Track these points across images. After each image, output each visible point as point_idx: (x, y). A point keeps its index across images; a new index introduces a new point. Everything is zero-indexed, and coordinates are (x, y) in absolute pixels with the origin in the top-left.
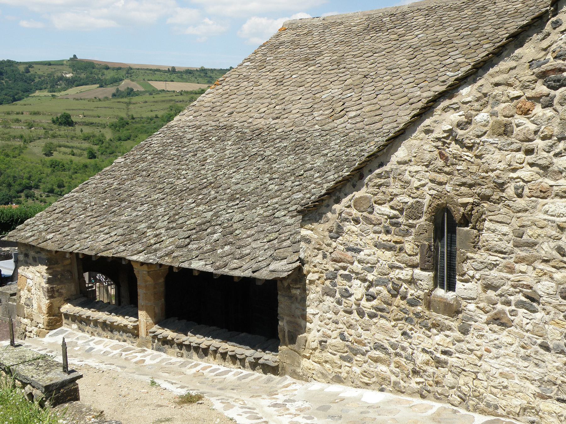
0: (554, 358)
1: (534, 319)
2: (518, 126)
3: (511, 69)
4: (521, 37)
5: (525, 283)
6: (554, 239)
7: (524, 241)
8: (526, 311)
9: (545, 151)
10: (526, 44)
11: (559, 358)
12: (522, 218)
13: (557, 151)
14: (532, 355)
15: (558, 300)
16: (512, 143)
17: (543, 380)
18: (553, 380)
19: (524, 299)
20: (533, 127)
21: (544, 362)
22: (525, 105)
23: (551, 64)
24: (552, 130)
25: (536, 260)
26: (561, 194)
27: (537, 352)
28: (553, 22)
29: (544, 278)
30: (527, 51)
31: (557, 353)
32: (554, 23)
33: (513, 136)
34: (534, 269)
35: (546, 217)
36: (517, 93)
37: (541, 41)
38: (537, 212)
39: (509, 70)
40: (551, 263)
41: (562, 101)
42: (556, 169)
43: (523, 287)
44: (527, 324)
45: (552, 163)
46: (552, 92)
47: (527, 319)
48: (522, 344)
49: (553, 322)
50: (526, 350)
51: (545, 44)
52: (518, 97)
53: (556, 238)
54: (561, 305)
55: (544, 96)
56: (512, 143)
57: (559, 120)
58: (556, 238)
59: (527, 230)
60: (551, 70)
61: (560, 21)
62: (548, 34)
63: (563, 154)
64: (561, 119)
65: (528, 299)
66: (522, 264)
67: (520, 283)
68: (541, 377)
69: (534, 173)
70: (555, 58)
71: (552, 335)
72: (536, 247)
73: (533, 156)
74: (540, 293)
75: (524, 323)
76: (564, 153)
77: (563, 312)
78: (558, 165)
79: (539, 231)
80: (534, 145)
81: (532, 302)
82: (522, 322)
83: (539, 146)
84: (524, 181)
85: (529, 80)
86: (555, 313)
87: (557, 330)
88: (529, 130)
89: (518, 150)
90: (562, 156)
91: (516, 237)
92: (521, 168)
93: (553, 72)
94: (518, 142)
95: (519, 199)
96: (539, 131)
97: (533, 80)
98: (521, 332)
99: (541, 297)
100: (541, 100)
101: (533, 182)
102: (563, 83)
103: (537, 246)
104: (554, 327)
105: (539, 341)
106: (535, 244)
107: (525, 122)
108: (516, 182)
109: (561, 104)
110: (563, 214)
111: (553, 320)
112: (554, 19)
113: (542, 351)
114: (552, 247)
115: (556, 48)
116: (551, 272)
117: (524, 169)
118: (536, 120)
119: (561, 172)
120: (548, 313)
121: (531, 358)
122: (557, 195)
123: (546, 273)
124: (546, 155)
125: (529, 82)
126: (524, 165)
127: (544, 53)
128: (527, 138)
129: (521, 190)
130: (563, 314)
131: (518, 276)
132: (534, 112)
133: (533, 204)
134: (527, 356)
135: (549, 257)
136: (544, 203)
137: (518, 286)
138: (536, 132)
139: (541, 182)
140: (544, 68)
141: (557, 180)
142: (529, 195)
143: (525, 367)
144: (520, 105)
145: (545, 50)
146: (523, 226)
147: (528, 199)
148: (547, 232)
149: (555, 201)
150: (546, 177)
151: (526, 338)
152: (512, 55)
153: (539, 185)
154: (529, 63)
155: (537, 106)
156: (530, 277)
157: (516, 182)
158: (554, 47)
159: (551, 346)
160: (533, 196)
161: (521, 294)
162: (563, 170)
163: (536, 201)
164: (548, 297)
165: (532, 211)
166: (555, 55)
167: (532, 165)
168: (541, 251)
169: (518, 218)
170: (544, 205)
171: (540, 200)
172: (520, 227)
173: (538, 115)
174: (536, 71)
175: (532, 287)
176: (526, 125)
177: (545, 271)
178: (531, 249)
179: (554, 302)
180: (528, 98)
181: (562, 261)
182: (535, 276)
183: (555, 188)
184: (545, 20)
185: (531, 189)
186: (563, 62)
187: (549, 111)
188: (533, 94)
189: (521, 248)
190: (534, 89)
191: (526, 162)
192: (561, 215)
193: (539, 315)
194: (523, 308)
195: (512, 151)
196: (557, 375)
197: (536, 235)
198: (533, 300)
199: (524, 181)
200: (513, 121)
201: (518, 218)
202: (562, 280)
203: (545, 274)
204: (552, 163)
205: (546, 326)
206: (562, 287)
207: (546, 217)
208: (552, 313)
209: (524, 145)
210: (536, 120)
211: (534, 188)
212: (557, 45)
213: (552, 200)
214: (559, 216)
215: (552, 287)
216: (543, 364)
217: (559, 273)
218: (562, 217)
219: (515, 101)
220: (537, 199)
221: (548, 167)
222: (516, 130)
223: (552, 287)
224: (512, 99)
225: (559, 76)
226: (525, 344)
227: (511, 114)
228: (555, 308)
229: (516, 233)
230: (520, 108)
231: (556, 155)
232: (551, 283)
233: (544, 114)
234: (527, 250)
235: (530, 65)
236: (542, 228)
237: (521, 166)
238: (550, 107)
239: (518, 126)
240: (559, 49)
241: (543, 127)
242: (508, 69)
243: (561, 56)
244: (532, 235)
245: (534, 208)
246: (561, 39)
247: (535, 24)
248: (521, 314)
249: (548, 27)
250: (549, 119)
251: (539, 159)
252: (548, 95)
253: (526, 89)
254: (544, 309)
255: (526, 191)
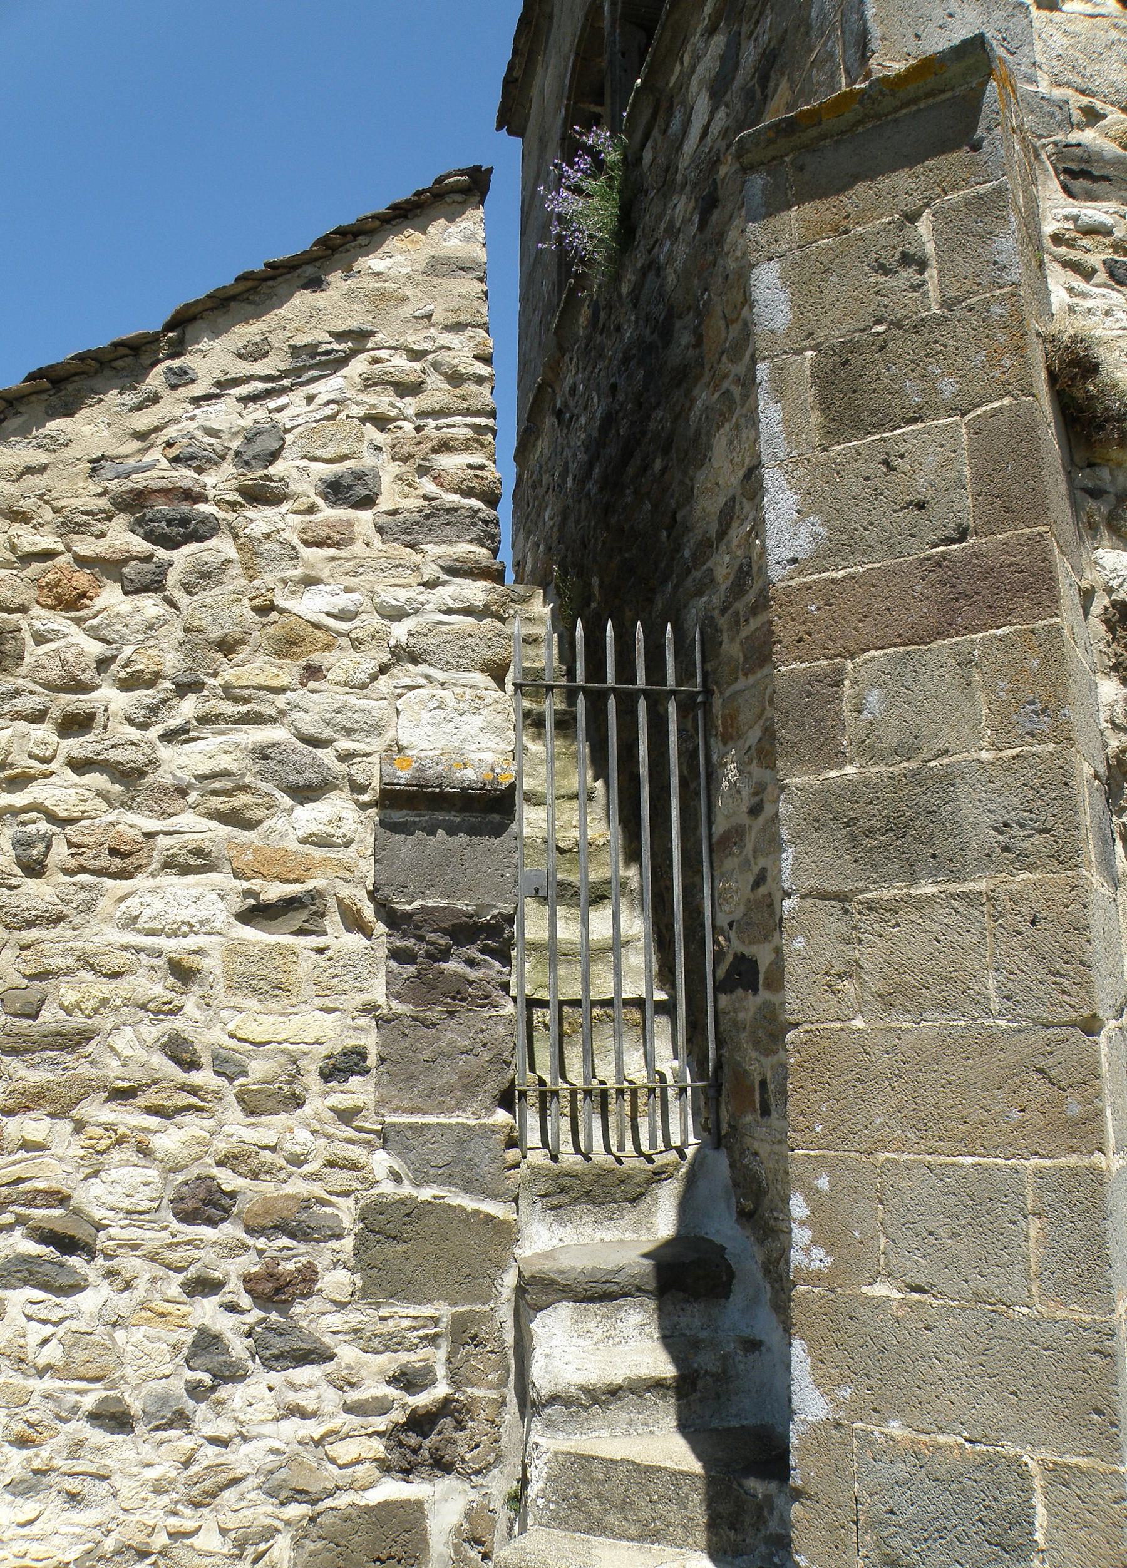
0: (147, 1452)
1: (72, 1317)
2: (40, 639)
3: (30, 470)
4: (70, 387)
5: (41, 1185)
6: (157, 1013)
7: (43, 1030)
8: (38, 1295)
9: (129, 720)
10: (84, 412)
11: (163, 1448)
12: (40, 947)
13: (174, 723)
14: (58, 1462)
15: (166, 1228)
16: (18, 693)
17: (99, 1552)
18: (138, 1539)
19: (33, 1248)
20: (96, 649)
21: (104, 1478)
22: (69, 580)
23: (162, 473)
24: (157, 659)
25: (85, 1096)
26: (185, 858)
27: (80, 1444)
28: (170, 369)
29: (116, 1155)
30: (86, 430)
31: (157, 1428)
32: (175, 374)
33: (23, 670)
34: (79, 1126)
35: (130, 938)
36: (47, 541)
37: (130, 410)
38: (95, 924)
39: (22, 474)
40: (141, 1101)
41: (192, 578)
42: (168, 781)
43: (30, 1204)
44: (45, 1342)
45: (154, 763)
46: (161, 554)
47: (44, 1322)
48: (18, 1427)
49: (143, 1314)
50: (30, 1453)
51: (143, 421)
52: (47, 555)
53: (166, 1007)
54: (178, 1244)
55: (136, 558)
56: (18, 693)
57: (180, 634)
58: (166, 1007)
59: (57, 987)
60: (159, 491)
61: (190, 371)
62: (155, 399)
63: (192, 734)
64: (187, 630)
65: (47, 1244)
66: (34, 1114)
67: (23, 1187)
68: (91, 1545)
69: (90, 795)
70: (176, 460)
71: (141, 1362)
72: (90, 1047)
73: (90, 737)
74: (98, 1214)
75: (33, 1339)
76: (195, 729)
77: (179, 1270)
78: (174, 767)
79: (106, 988)
80: (96, 705)
81: (63, 1253)
82: (22, 1342)
83: (112, 708)
84: (52, 818)
85: (85, 508)
86: (153, 1280)
87: (159, 1339)
88: (80, 654)
89: (38, 717)
90: (187, 741)
91: (15, 1015)
92: (46, 776)
93: (166, 496)
94: (39, 689)
95: (31, 882)
96: (114, 658)
97: (103, 511)
98: (18, 1380)
99: (99, 1227)
100: (125, 570)
101: (83, 823)
102: (195, 531)
103: (93, 1043)
104: (152, 1332)
105: (89, 1402)
106: (86, 1036)
107: (66, 630)
108: (23, 824)
109: (188, 589)
110: (192, 926)
111: (143, 1306)
112: (175, 363)
113: (98, 1436)
114: (150, 1042)
115: (176, 437)
116: (145, 1130)
117: (54, 779)
118: (108, 625)
119: (183, 792)
120: (128, 1286)
121: (53, 1478)
122: (170, 864)
123: (124, 1136)
124: (135, 734)
125: (87, 513)
126: (54, 765)
127: (137, 445)
128: (73, 678)
129: (41, 847)
130: (181, 1277)
131: (14, 1164)
132: (99, 603)
133: (83, 895)
134: (36, 1472)
135: (138, 1076)
136: (121, 893)
137: (13, 1203)
138: (103, 664)
139: (113, 824)
140: (139, 481)
141: (170, 815)
142: (72, 864)
143: (23, 1525)
144: (50, 577)
145: (141, 436)
146: (42, 976)
147: (67, 879)
148: (133, 990)
149: (164, 883)
150: (131, 808)
151: (35, 1401)
152: (34, 433)
153: (106, 831)
154: (90, 462)
155: (108, 589)
156: (61, 1159)
157: (23, 824)
158: (171, 432)
159: (136, 1407)
160: (83, 870)
161: (19, 1232)
162: (190, 785)
163: (92, 887)
164: (129, 1226)
165: (77, 920)
166: (173, 452)
167: (80, 766)
168: (107, 1060)
169: (23, 948)
170: (121, 900)
171: (109, 883)
172: (30, 978)
173: (116, 610)
174: (113, 487)
175: (69, 1197)
176: (69, 639)
177: (122, 1130)
178: (69, 1058)
179: (153, 1238)
180: (82, 561)
181: (182, 1088)
182: (82, 1152)
183: (162, 840)
184: (146, 360)
185: (79, 846)
186: (196, 476)
187: (151, 602)
188: (98, 550)
189: (28, 1057)
190: (102, 535)
191: (60, 759)
192: (185, 929)
193: (88, 1301)
194: (25, 1283)
195: (17, 716)
196: (154, 1513)
197: (92, 1004)
198: (67, 1244)
199: (52, 818)
200: (24, 625)
201: (23, 948)
202: (185, 1152)
203: (120, 1141)
204: (154, 763)
205: (120, 1335)
206: (180, 1178)
207: (130, 938)
208: (142, 1284)
209: (58, 702)
210: (108, 625)
211: (89, 840)
212: (180, 431)
213: (151, 883)
214: (174, 934)
215: (146, 1184)
216: (101, 1488)
217: (173, 1130)
218: (185, 935)
219: (35, 565)
220: (98, 880)
221: (142, 774)
222: (33, 653)
223: (146, 1184)
224: (27, 559)
225: (185, 508)
226: (31, 1425)
227: (18, 601)
228: (153, 1260)
229: (13, 1002)
230: (50, 586)
231: (168, 737)
232: (140, 1170)
233: (137, 609)
234: (53, 1063)
235: (94, 470)
236: (115, 975)
237: (44, 767)
238: (155, 591)
239: (40, 639)
240: (186, 441)
241: (127, 651)
242: (20, 469)
243: (193, 457)
244: (78, 1006)
245: (88, 908)
246: (192, 418)
247: (119, 363)
248: (19, 1309)
249: (155, 380)
250: (151, 627)
251: (113, 746)
252: (148, 559)
253: (77, 533)
254: (110, 1274)
255: (60, 852)
